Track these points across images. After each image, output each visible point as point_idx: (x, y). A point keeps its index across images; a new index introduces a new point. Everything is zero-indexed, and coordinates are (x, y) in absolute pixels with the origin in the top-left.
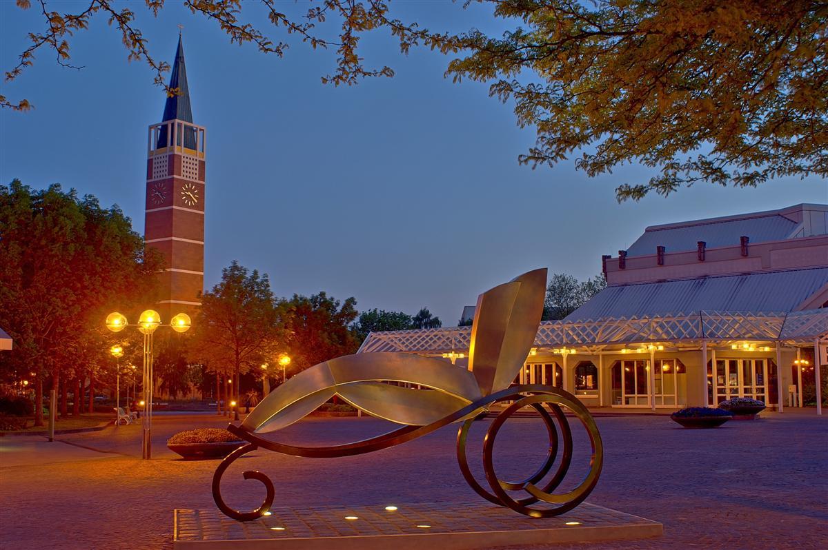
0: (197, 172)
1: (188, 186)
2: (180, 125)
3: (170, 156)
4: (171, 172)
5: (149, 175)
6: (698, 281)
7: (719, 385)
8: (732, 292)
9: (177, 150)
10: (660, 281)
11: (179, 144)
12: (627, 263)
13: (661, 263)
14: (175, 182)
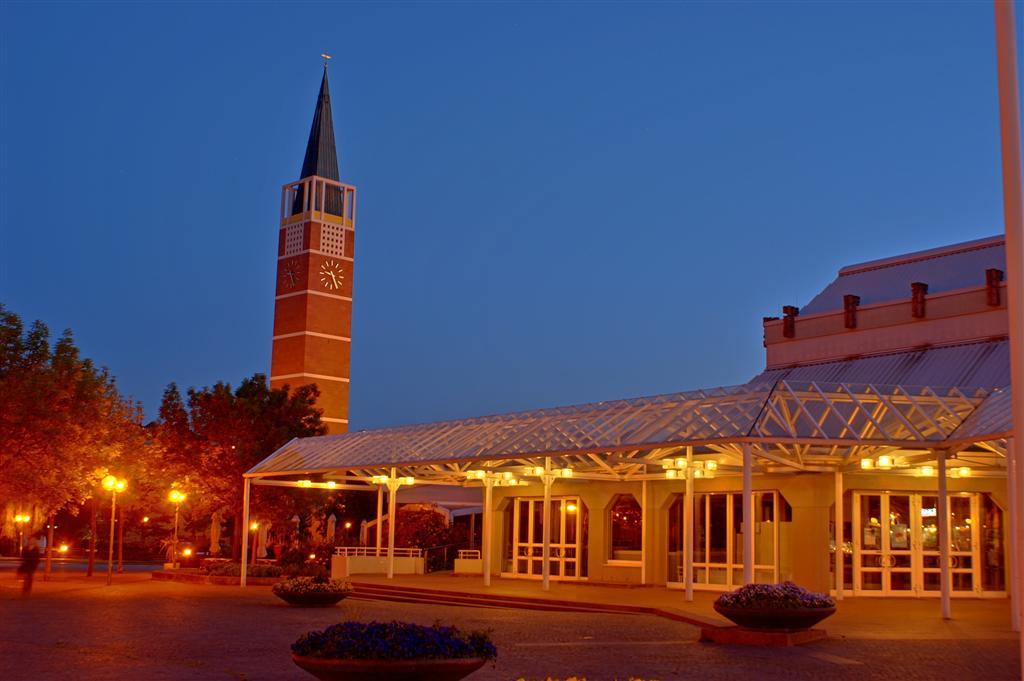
0: (343, 245)
1: (330, 263)
2: (319, 184)
3: (306, 224)
4: (307, 246)
5: (281, 251)
6: (912, 354)
7: (864, 547)
8: (965, 373)
9: (315, 217)
10: (851, 358)
11: (318, 209)
12: (797, 326)
13: (851, 323)
14: (311, 258)
